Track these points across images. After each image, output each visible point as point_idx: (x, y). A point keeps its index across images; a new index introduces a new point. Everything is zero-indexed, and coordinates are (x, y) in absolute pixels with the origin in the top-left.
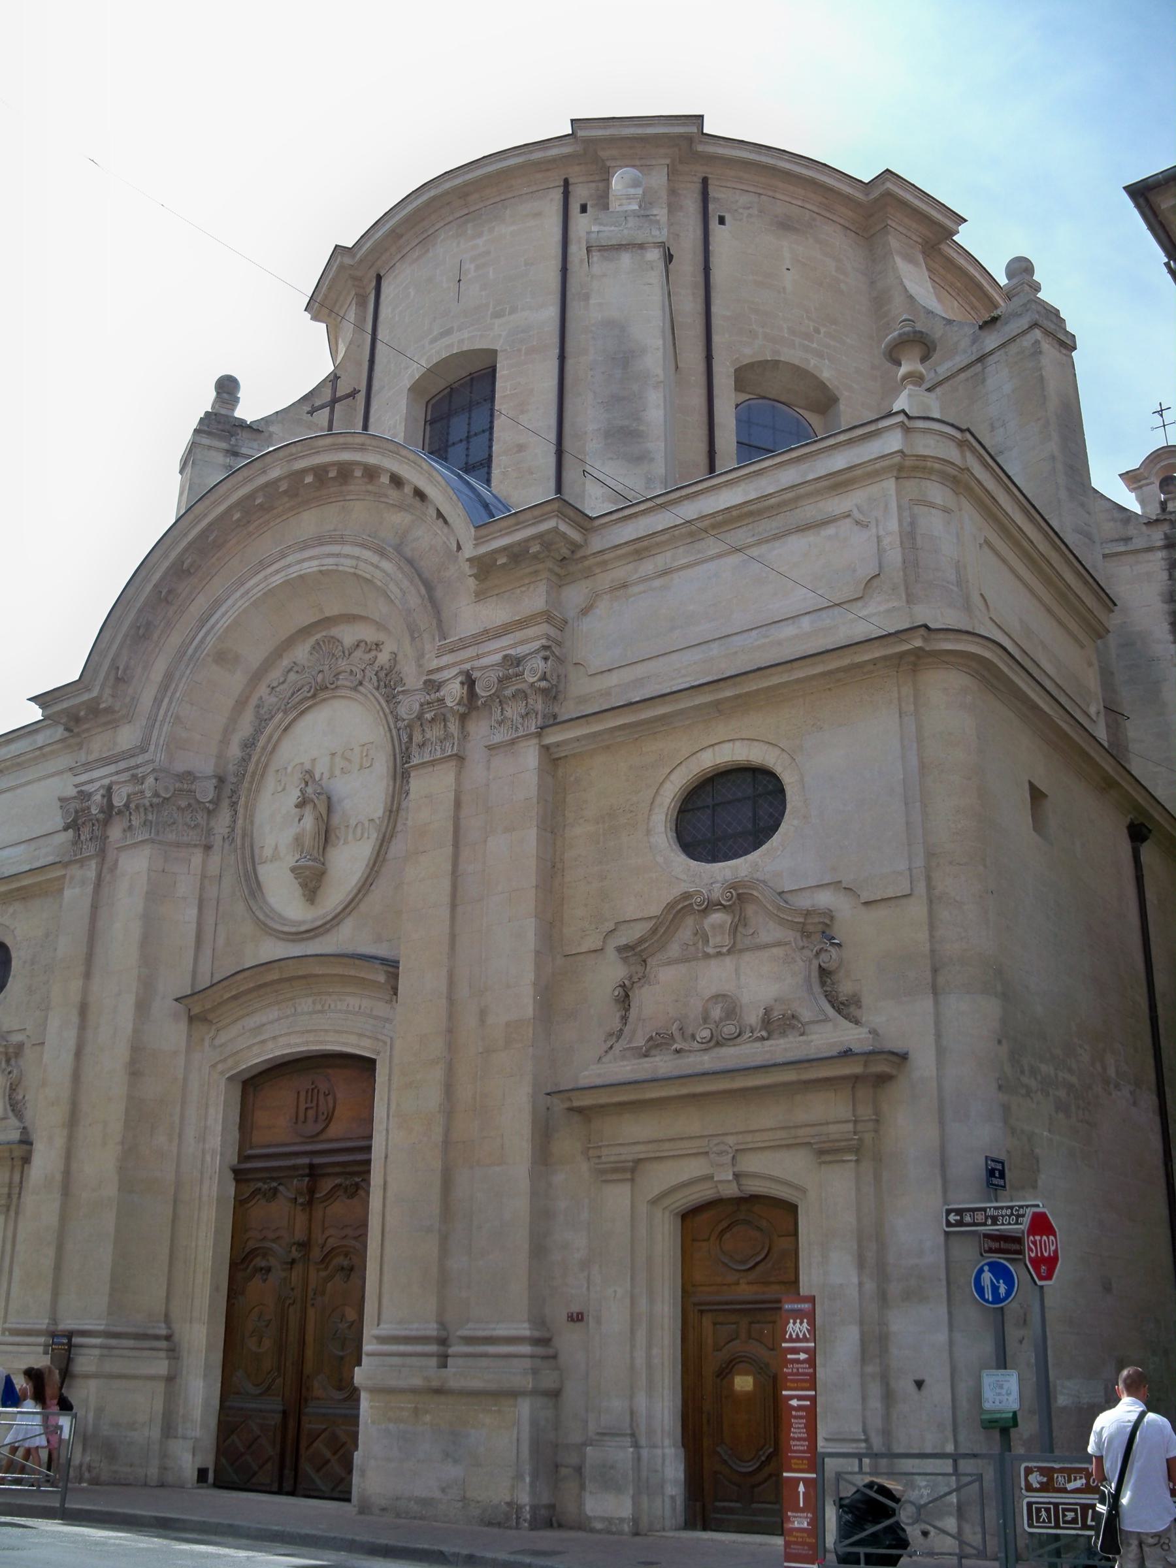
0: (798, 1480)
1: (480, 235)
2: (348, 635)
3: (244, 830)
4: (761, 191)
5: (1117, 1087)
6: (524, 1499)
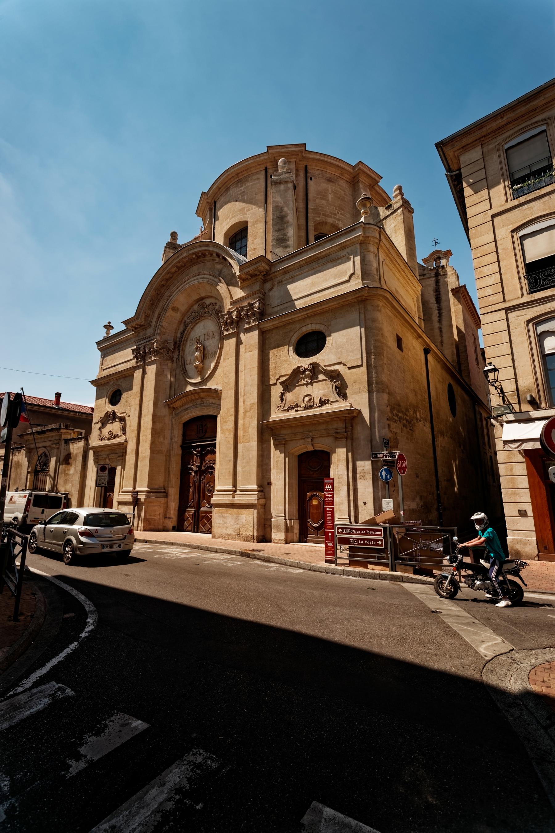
0: (329, 532)
1: (242, 186)
2: (208, 301)
3: (182, 356)
4: (322, 169)
5: (420, 421)
6: (255, 534)
